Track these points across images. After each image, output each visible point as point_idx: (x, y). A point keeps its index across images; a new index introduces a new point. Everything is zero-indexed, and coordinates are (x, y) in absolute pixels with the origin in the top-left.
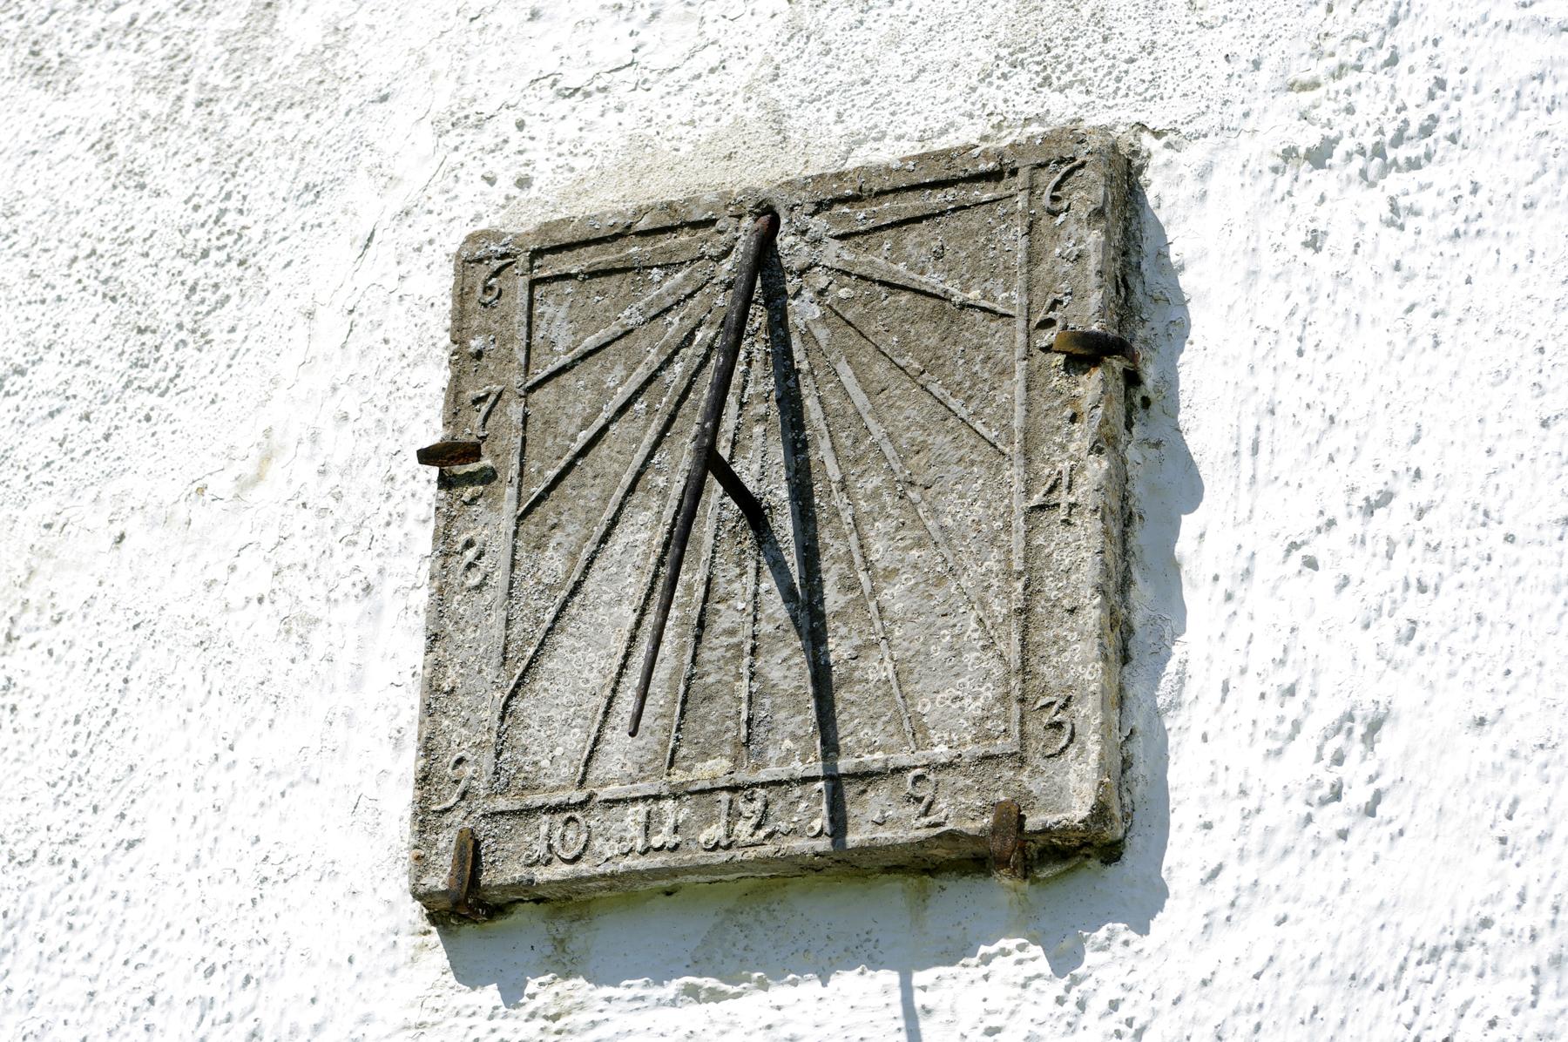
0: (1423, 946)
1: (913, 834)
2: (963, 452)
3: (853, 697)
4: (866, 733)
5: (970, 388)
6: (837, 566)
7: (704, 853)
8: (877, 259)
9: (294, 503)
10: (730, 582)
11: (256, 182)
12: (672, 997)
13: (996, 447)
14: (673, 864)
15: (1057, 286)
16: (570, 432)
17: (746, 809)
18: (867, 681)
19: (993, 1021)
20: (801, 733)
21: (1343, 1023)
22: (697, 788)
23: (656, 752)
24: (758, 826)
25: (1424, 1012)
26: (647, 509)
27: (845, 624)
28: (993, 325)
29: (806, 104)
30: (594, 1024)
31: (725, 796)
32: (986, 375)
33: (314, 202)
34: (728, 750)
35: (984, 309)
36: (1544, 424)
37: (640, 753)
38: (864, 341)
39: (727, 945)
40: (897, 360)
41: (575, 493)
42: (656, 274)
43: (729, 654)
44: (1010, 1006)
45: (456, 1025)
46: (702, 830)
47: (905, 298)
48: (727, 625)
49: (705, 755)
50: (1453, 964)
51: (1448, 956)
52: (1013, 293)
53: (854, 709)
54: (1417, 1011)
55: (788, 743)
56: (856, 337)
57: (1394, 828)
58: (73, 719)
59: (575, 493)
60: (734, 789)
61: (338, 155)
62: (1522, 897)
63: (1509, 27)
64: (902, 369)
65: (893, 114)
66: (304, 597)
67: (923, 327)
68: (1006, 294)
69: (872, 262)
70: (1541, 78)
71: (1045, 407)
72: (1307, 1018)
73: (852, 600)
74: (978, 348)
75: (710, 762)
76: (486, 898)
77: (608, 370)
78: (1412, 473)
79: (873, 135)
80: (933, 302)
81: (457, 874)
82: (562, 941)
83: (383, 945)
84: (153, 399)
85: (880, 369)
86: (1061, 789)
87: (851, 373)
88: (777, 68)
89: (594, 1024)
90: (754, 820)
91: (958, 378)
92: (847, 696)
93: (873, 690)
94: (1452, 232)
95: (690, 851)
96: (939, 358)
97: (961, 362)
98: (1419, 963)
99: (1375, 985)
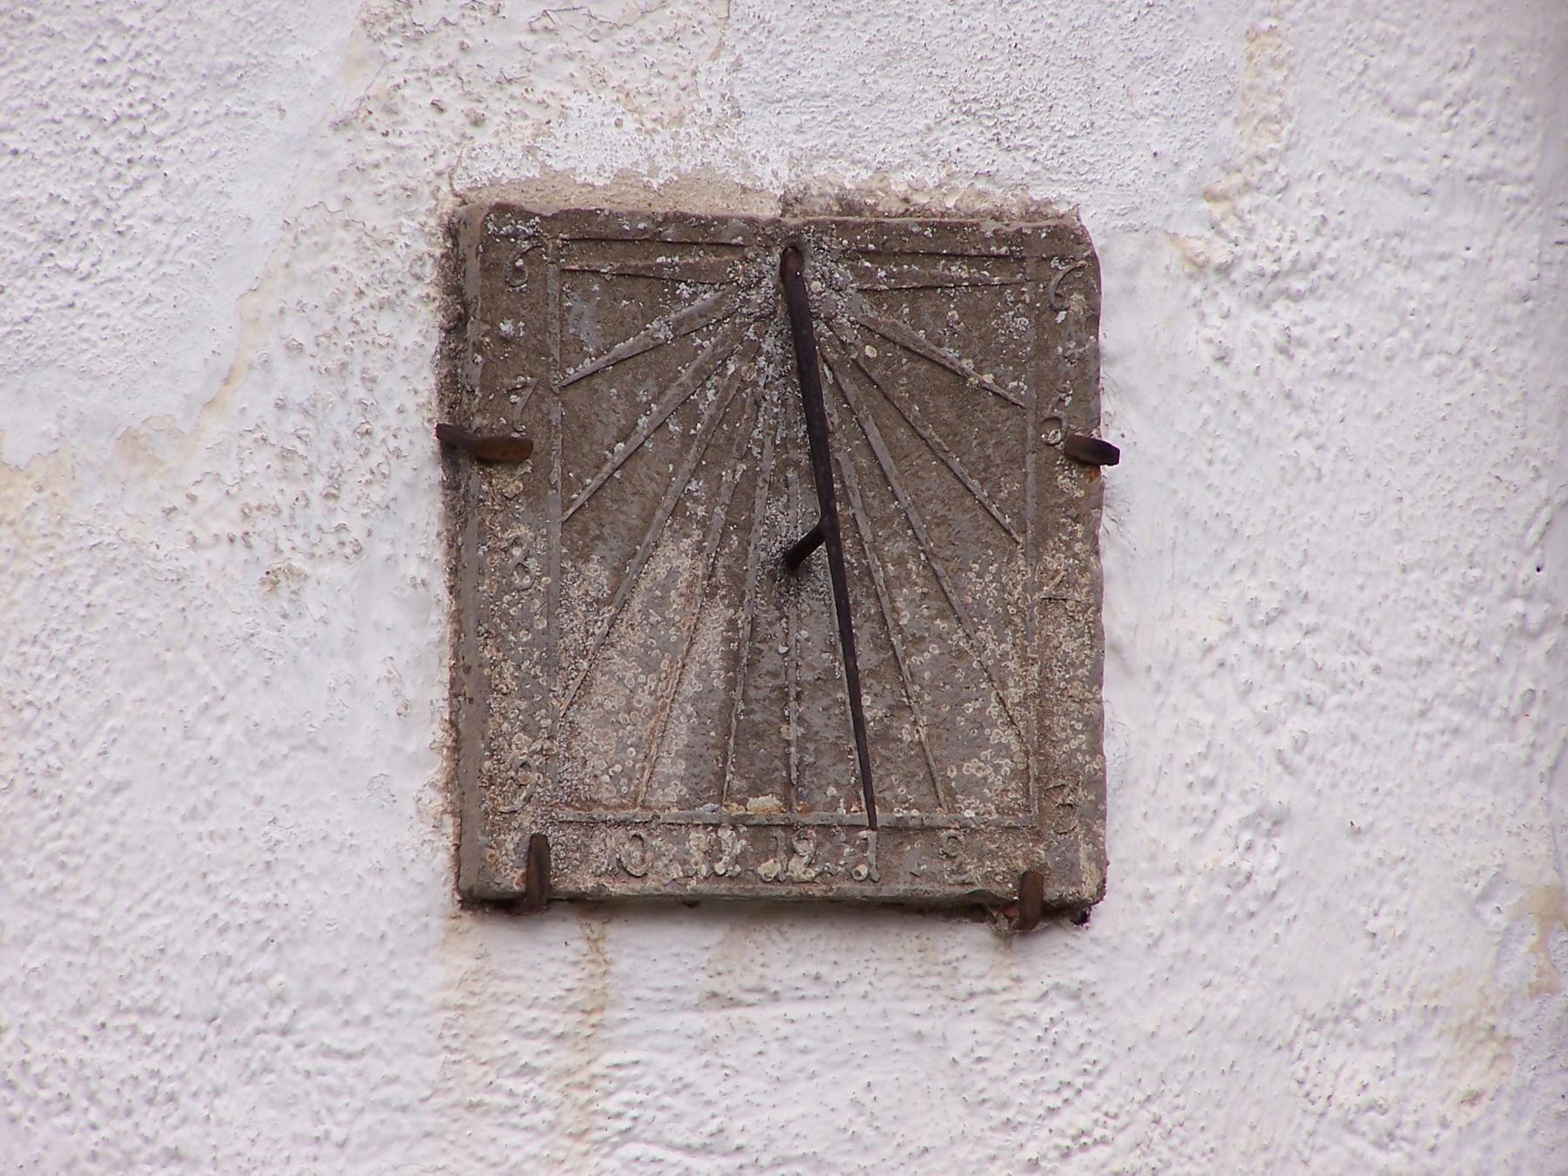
0: (1313, 1017)
1: (948, 890)
2: (980, 532)
3: (888, 754)
4: (901, 791)
5: (984, 470)
6: (869, 624)
7: (763, 885)
8: (899, 319)
9: (251, 437)
10: (771, 624)
11: (169, 47)
12: (695, 1002)
13: (1011, 534)
14: (737, 892)
15: (1060, 385)
16: (606, 442)
17: (800, 847)
18: (900, 740)
19: (981, 1053)
20: (843, 781)
21: (1252, 1075)
22: (755, 822)
23: (710, 781)
24: (809, 865)
25: (1313, 1071)
26: (688, 536)
27: (879, 683)
28: (1003, 411)
29: (600, 19)
30: (625, 1021)
31: (780, 833)
32: (999, 461)
33: (236, 86)
34: (778, 789)
35: (995, 394)
36: (1404, 570)
37: (694, 780)
38: (887, 404)
39: (745, 960)
40: (920, 430)
41: (615, 507)
42: (684, 290)
43: (773, 695)
44: (997, 1039)
45: (495, 1011)
46: (759, 863)
47: (924, 367)
48: (770, 667)
49: (756, 791)
50: (1331, 1034)
51: (1329, 1027)
52: (1021, 384)
53: (890, 766)
54: (1307, 1069)
55: (832, 791)
56: (881, 398)
57: (1290, 914)
58: (30, 639)
59: (615, 507)
60: (788, 827)
61: (261, 38)
62: (1386, 983)
63: (1378, 178)
64: (922, 438)
65: (851, 136)
66: (284, 546)
67: (944, 401)
68: (1015, 384)
69: (894, 324)
70: (1399, 235)
71: (1052, 503)
72: (1227, 1070)
73: (884, 660)
74: (990, 431)
75: (761, 798)
76: (559, 892)
77: (641, 382)
78: (1302, 596)
79: (831, 154)
80: (950, 377)
81: (526, 877)
82: (596, 941)
83: (413, 927)
84: (73, 285)
85: (902, 433)
86: (1073, 864)
87: (878, 434)
88: (739, 58)
89: (625, 1021)
90: (806, 859)
91: (973, 459)
92: (883, 752)
93: (907, 750)
94: (1330, 370)
95: (749, 882)
96: (956, 435)
97: (975, 443)
98: (1308, 1031)
99: (1275, 1045)
